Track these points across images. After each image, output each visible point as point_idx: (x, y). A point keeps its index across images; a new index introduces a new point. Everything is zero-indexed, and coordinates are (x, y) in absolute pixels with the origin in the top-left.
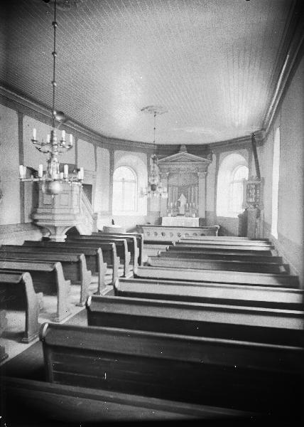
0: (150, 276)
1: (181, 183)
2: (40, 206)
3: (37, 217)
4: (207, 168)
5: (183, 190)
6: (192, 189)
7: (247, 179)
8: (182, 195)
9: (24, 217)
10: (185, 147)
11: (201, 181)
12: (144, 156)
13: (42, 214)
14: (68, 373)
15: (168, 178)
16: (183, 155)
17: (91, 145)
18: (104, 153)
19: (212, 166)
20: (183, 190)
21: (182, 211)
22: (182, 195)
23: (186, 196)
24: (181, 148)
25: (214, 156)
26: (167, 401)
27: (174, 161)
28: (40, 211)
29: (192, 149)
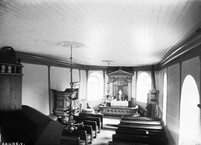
0: (112, 92)
1: (119, 84)
2: (57, 106)
3: (56, 112)
4: (132, 78)
5: (120, 88)
6: (125, 87)
7: (151, 90)
8: (120, 90)
9: (51, 112)
10: (121, 68)
11: (129, 84)
12: (102, 72)
13: (59, 110)
14: (61, 61)
15: (113, 82)
16: (120, 71)
17: (78, 70)
18: (83, 72)
19: (134, 77)
20: (120, 88)
21: (120, 98)
22: (120, 90)
23: (122, 91)
24: (120, 68)
25: (135, 72)
26: (135, 127)
27: (116, 74)
28: (57, 109)
29: (125, 69)
